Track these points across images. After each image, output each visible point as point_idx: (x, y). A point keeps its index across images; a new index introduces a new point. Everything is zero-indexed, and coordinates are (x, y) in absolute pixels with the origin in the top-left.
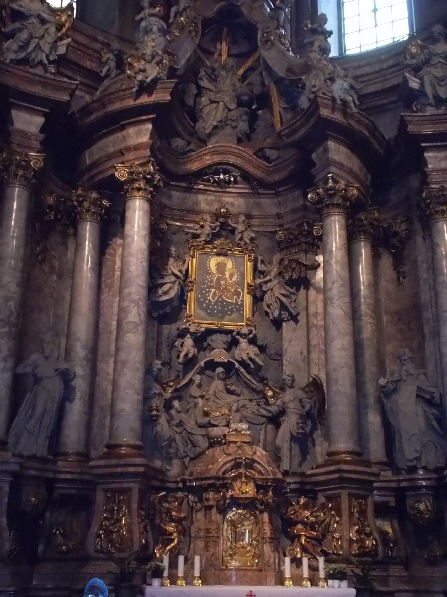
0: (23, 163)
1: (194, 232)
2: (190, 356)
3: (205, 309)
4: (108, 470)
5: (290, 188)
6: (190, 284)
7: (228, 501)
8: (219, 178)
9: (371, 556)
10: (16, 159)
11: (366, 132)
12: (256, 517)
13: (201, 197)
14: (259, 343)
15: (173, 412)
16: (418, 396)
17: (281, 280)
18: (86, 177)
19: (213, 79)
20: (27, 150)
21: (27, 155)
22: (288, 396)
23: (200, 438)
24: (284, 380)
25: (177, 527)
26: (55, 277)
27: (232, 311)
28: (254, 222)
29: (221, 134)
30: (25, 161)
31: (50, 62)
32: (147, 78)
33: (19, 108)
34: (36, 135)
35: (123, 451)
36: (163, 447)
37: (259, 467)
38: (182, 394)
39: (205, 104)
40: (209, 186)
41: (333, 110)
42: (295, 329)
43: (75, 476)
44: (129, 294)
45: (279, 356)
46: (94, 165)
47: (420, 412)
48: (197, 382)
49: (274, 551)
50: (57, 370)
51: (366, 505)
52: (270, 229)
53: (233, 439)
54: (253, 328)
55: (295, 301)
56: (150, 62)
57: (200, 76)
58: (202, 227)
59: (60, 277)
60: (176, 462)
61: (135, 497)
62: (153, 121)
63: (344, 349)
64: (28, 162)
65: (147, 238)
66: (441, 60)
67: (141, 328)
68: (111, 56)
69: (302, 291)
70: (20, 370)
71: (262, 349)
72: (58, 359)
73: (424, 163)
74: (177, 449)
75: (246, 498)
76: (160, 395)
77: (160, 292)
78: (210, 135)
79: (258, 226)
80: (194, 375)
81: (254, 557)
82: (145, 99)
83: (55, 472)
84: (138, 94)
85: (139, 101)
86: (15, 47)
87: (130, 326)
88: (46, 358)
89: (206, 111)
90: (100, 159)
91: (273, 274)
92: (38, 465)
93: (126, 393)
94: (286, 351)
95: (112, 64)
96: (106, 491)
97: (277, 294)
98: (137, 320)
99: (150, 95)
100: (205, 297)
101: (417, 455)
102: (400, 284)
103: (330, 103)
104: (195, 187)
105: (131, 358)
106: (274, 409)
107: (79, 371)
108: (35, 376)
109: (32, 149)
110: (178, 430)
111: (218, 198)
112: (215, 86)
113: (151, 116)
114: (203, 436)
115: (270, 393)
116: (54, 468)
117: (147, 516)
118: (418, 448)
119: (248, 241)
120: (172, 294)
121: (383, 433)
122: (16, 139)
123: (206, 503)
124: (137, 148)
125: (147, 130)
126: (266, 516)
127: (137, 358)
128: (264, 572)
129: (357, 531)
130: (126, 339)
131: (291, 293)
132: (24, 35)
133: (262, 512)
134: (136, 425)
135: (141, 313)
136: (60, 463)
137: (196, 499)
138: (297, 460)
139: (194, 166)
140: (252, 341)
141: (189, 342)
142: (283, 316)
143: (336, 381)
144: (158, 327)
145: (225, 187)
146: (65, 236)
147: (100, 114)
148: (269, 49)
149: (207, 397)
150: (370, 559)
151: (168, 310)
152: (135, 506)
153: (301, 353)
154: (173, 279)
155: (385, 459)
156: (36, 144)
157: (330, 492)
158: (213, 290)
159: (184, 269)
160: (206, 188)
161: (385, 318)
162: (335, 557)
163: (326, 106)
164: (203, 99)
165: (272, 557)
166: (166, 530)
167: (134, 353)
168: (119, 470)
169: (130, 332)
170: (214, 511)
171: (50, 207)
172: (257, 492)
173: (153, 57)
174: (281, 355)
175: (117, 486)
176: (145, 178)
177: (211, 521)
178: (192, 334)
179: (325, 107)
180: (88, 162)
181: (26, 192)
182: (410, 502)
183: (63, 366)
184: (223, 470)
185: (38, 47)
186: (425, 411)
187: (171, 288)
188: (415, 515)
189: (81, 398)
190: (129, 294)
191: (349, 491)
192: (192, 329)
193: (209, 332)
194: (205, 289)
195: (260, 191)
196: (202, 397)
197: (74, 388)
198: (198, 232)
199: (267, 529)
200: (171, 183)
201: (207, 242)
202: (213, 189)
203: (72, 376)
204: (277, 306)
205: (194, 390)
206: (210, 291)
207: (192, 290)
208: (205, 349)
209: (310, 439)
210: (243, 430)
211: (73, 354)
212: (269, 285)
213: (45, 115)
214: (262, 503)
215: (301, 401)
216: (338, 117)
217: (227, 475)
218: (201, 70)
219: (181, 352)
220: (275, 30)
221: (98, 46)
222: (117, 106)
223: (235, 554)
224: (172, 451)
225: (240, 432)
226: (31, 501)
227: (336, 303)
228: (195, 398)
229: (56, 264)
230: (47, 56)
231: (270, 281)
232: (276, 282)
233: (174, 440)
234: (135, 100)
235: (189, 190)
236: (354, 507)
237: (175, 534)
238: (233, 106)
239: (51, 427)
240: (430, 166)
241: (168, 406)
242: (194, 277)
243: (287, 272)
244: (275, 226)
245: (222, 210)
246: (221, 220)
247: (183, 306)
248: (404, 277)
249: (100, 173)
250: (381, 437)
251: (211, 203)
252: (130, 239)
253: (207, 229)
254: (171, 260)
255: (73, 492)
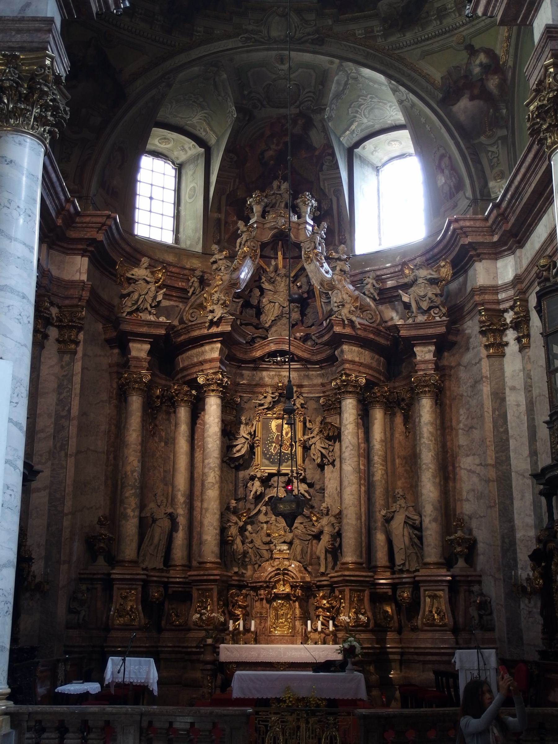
0: (139, 380)
1: (259, 402)
2: (258, 493)
3: (268, 459)
4: (199, 578)
5: (329, 365)
6: (257, 442)
7: (273, 595)
8: (277, 360)
9: (364, 627)
10: (133, 377)
11: (371, 336)
12: (290, 604)
13: (265, 373)
14: (308, 481)
15: (247, 533)
16: (405, 522)
17: (322, 436)
18: (180, 376)
19: (272, 282)
20: (139, 370)
21: (140, 374)
22: (324, 521)
23: (265, 552)
24: (322, 510)
25: (242, 611)
26: (163, 444)
27: (288, 459)
28: (305, 390)
29: (278, 324)
30: (139, 378)
31: (151, 307)
32: (215, 317)
33: (134, 341)
34: (146, 359)
35: (208, 565)
36: (239, 559)
37: (292, 574)
38: (254, 520)
39: (266, 303)
40: (270, 365)
41: (344, 326)
42: (333, 472)
43: (181, 580)
44: (209, 464)
45: (322, 490)
46: (185, 369)
47: (406, 533)
48: (264, 512)
49: (302, 625)
50: (165, 514)
51: (364, 596)
52: (317, 395)
53: (277, 556)
54: (302, 472)
55: (333, 450)
56: (217, 304)
57: (262, 281)
58: (265, 397)
59: (166, 443)
60: (249, 567)
61: (215, 594)
62: (221, 342)
63: (353, 495)
64: (141, 378)
65: (172, 547)
66: (424, 281)
67: (217, 486)
68: (196, 280)
69: (337, 444)
70: (143, 515)
71: (311, 485)
72: (166, 506)
73: (414, 355)
74: (251, 559)
75: (283, 594)
76: (236, 523)
77: (235, 450)
78: (270, 326)
79: (308, 393)
80: (261, 507)
81: (289, 629)
82: (214, 330)
83: (168, 578)
84: (210, 327)
85: (210, 331)
86: (129, 304)
87: (210, 485)
88: (159, 506)
89: (267, 308)
90: (188, 365)
91: (315, 432)
92: (157, 574)
93: (209, 529)
94: (327, 486)
95: (196, 284)
96: (198, 590)
97: (318, 447)
98: (214, 481)
99: (218, 327)
100: (268, 450)
101: (403, 562)
102: (407, 437)
103: (341, 322)
104: (261, 366)
105: (210, 506)
106: (315, 530)
107: (181, 511)
108: (153, 518)
109: (143, 368)
110: (250, 546)
111: (277, 373)
112: (274, 287)
113: (219, 339)
114: (267, 550)
115: (314, 518)
116: (168, 575)
117: (224, 605)
118: (404, 558)
119: (299, 406)
120: (243, 451)
121: (387, 546)
122: (132, 363)
123: (260, 597)
124: (212, 360)
125: (217, 348)
126: (297, 604)
127: (215, 506)
128: (295, 637)
129: (355, 612)
130: (207, 494)
131: (329, 445)
132: (135, 296)
133: (294, 602)
134: (216, 549)
135: (217, 476)
136: (171, 572)
137: (255, 594)
138: (330, 565)
139: (258, 354)
140: (304, 480)
141: (257, 483)
142: (325, 462)
143: (346, 516)
144: (236, 473)
145: (283, 365)
146: (168, 413)
147: (187, 336)
148: (310, 263)
149: (271, 522)
150: (363, 628)
151: (241, 462)
152: (215, 599)
153: (336, 489)
154: (243, 440)
155: (388, 564)
156: (146, 364)
157: (341, 588)
158: (274, 445)
159: (252, 430)
160: (268, 366)
161: (397, 461)
162: (341, 628)
163: (338, 325)
164: (264, 300)
165: (300, 629)
166: (235, 613)
167: (213, 503)
168: (205, 577)
169: (210, 489)
170: (264, 601)
171: (158, 397)
172: (291, 589)
173: (218, 301)
174: (324, 490)
175: (204, 587)
176: (216, 383)
177: (263, 607)
178: (259, 478)
179: (338, 326)
180: (181, 366)
181: (140, 398)
182: (398, 592)
183: (169, 510)
184: (269, 576)
185: (145, 300)
186: (409, 533)
187: (242, 447)
188: (401, 600)
189: (183, 529)
190: (209, 464)
191: (350, 587)
192: (259, 475)
193: (271, 475)
194: (268, 444)
195: (309, 366)
196: (267, 522)
197: (178, 523)
198: (262, 402)
199: (298, 612)
200: (243, 365)
201: (268, 409)
202: (273, 367)
203: (176, 516)
204: (319, 455)
205: (262, 518)
206: (272, 446)
207: (258, 446)
208: (270, 487)
209: (339, 551)
210: (284, 550)
211: (176, 500)
212: (313, 441)
213: (150, 343)
214: (295, 596)
215: (333, 525)
216: (348, 331)
217: (272, 580)
218: (263, 277)
219: (251, 491)
220: (313, 250)
221: (186, 272)
222: (196, 333)
223: (277, 627)
224: (247, 560)
225: (283, 551)
226: (155, 596)
227: (348, 462)
228: (262, 523)
229: (163, 434)
230: (150, 305)
231: (313, 437)
232: (318, 437)
233: (248, 552)
234: (208, 330)
235: (256, 369)
236: (354, 597)
237: (241, 615)
238: (286, 304)
239: (164, 550)
240: (418, 358)
241: (242, 530)
242: (259, 436)
243: (325, 430)
244: (320, 393)
245: (280, 385)
246: (280, 391)
247: (253, 457)
248: (409, 432)
249: (188, 375)
250: (386, 549)
251: (272, 378)
252: (208, 426)
253: (269, 399)
254: (242, 426)
255: (180, 589)
